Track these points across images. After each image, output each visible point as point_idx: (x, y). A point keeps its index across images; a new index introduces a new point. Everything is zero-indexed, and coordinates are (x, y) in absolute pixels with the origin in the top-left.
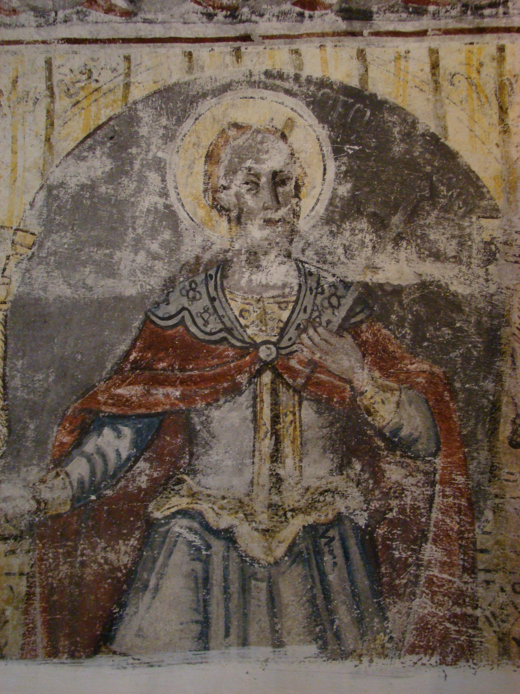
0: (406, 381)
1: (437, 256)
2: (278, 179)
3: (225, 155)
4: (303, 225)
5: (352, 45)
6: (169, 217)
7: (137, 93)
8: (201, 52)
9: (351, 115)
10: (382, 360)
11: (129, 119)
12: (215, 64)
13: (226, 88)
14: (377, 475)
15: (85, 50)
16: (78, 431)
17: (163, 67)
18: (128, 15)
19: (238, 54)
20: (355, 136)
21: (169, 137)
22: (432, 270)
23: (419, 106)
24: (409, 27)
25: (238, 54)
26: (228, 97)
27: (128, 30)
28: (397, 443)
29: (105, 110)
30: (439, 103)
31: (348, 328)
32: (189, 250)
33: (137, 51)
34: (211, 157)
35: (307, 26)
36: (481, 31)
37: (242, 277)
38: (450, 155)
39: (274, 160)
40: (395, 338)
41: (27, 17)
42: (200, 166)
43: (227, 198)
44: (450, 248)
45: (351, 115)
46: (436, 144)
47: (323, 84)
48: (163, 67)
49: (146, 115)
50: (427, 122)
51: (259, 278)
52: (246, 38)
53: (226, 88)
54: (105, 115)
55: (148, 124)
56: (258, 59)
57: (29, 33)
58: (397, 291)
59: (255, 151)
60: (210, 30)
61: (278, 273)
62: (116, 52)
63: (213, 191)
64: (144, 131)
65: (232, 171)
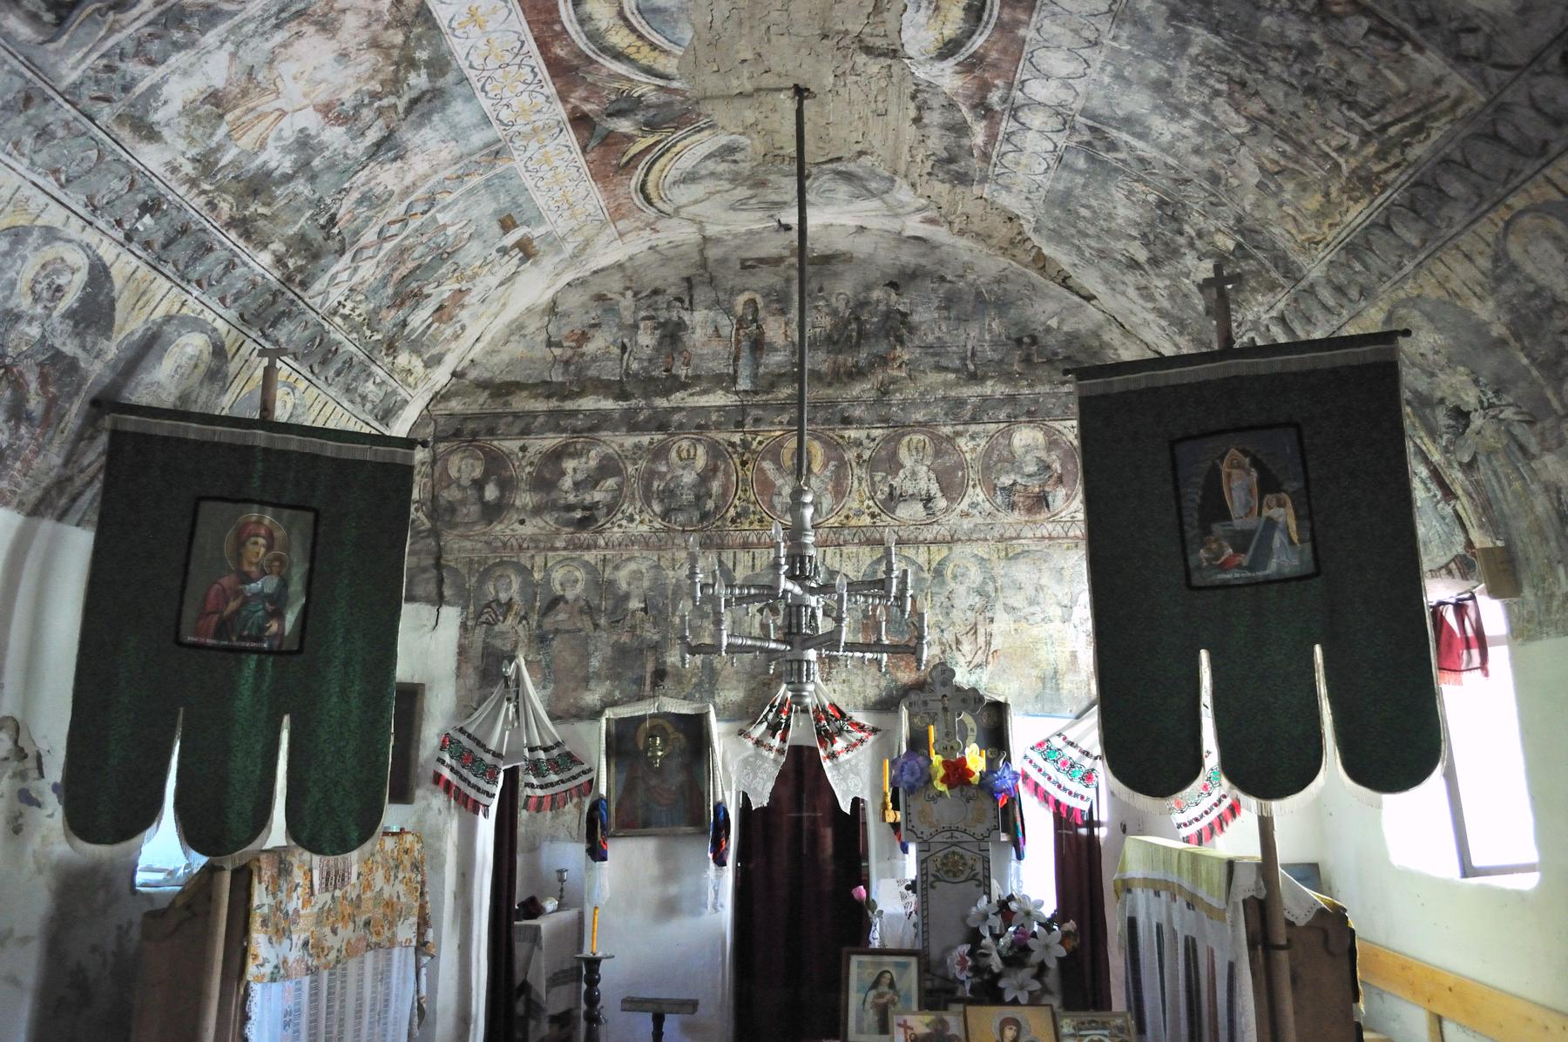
0: (45, 393)
1: (84, 348)
2: (59, 289)
3: (49, 268)
4: (55, 314)
5: (120, 249)
6: (12, 284)
7: (39, 222)
8: (73, 218)
9: (99, 274)
10: (44, 380)
11: (28, 231)
12: (74, 228)
13: (70, 241)
14: (17, 428)
15: (35, 190)
16: (101, 477)
17: (54, 216)
18: (62, 186)
19: (84, 229)
20: (255, 586)
21: (36, 249)
22: (80, 354)
23: (118, 282)
24: (138, 253)
25: (84, 229)
26: (69, 245)
27: (58, 193)
28: (29, 418)
29: (22, 221)
30: (124, 287)
31: (41, 365)
32: (11, 304)
33: (53, 204)
34: (44, 266)
35: (111, 232)
36: (155, 268)
37: (23, 327)
38: (113, 309)
39: (62, 281)
40: (54, 374)
41: (26, 161)
42: (37, 268)
43: (38, 287)
44: (89, 345)
45: (99, 274)
46: (112, 302)
47: (100, 259)
48: (54, 216)
49: (36, 233)
50: (115, 294)
51: (27, 329)
52: (91, 224)
53: (70, 241)
54: (21, 222)
55: (33, 240)
56: (91, 237)
57: (21, 169)
58: (66, 357)
59: (58, 272)
60: (82, 211)
61: (34, 331)
62: (44, 199)
63: (35, 281)
64: (30, 240)
65: (46, 276)
